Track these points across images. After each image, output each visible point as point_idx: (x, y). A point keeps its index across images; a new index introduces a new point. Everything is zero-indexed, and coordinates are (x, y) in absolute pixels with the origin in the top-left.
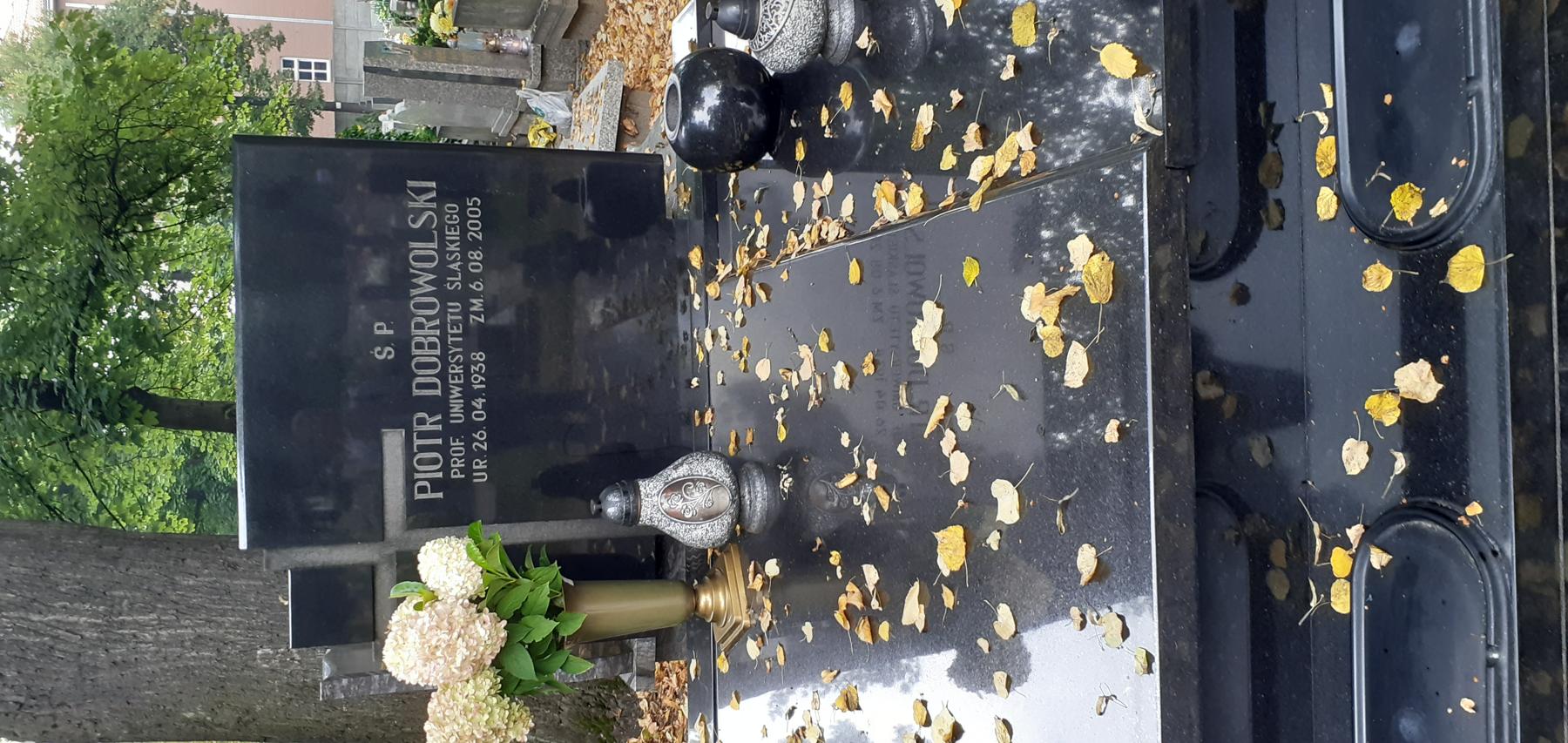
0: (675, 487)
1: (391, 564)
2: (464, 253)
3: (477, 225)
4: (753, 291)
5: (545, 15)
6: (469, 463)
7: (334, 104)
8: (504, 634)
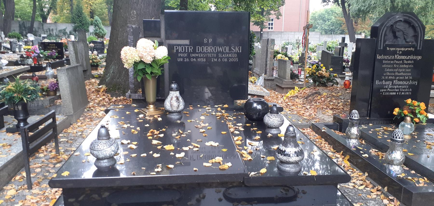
0: (178, 99)
1: (160, 41)
2: (226, 57)
3: (232, 60)
4: (219, 116)
5: (281, 80)
6: (182, 57)
7: (262, 31)
8: (148, 63)
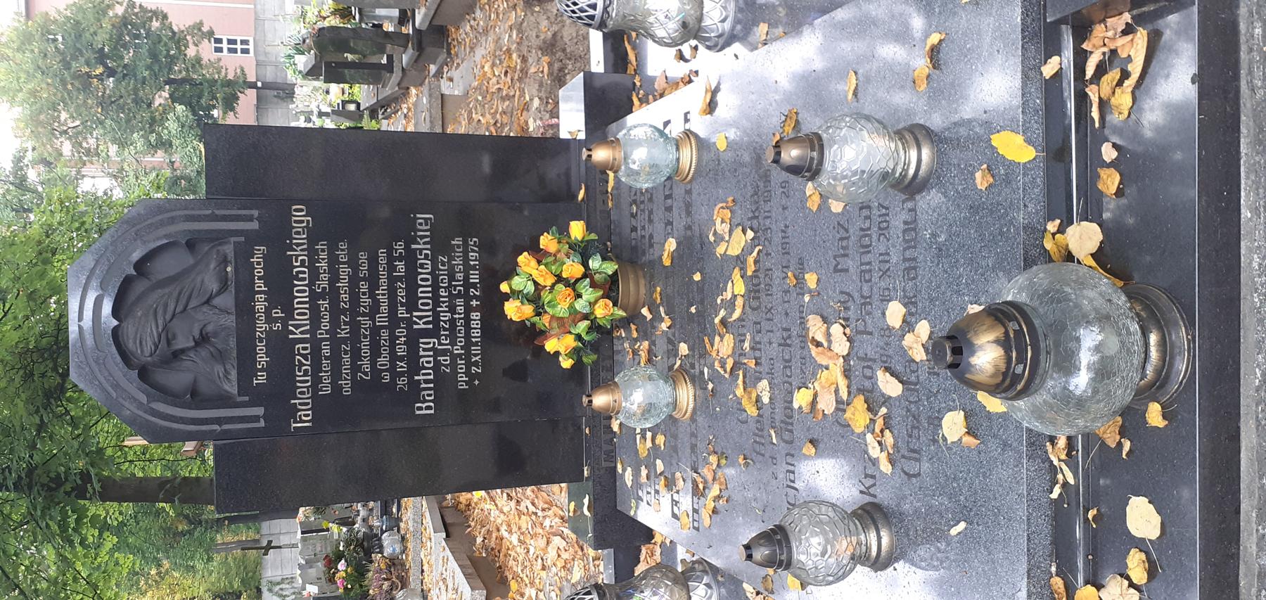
7: (256, 83)
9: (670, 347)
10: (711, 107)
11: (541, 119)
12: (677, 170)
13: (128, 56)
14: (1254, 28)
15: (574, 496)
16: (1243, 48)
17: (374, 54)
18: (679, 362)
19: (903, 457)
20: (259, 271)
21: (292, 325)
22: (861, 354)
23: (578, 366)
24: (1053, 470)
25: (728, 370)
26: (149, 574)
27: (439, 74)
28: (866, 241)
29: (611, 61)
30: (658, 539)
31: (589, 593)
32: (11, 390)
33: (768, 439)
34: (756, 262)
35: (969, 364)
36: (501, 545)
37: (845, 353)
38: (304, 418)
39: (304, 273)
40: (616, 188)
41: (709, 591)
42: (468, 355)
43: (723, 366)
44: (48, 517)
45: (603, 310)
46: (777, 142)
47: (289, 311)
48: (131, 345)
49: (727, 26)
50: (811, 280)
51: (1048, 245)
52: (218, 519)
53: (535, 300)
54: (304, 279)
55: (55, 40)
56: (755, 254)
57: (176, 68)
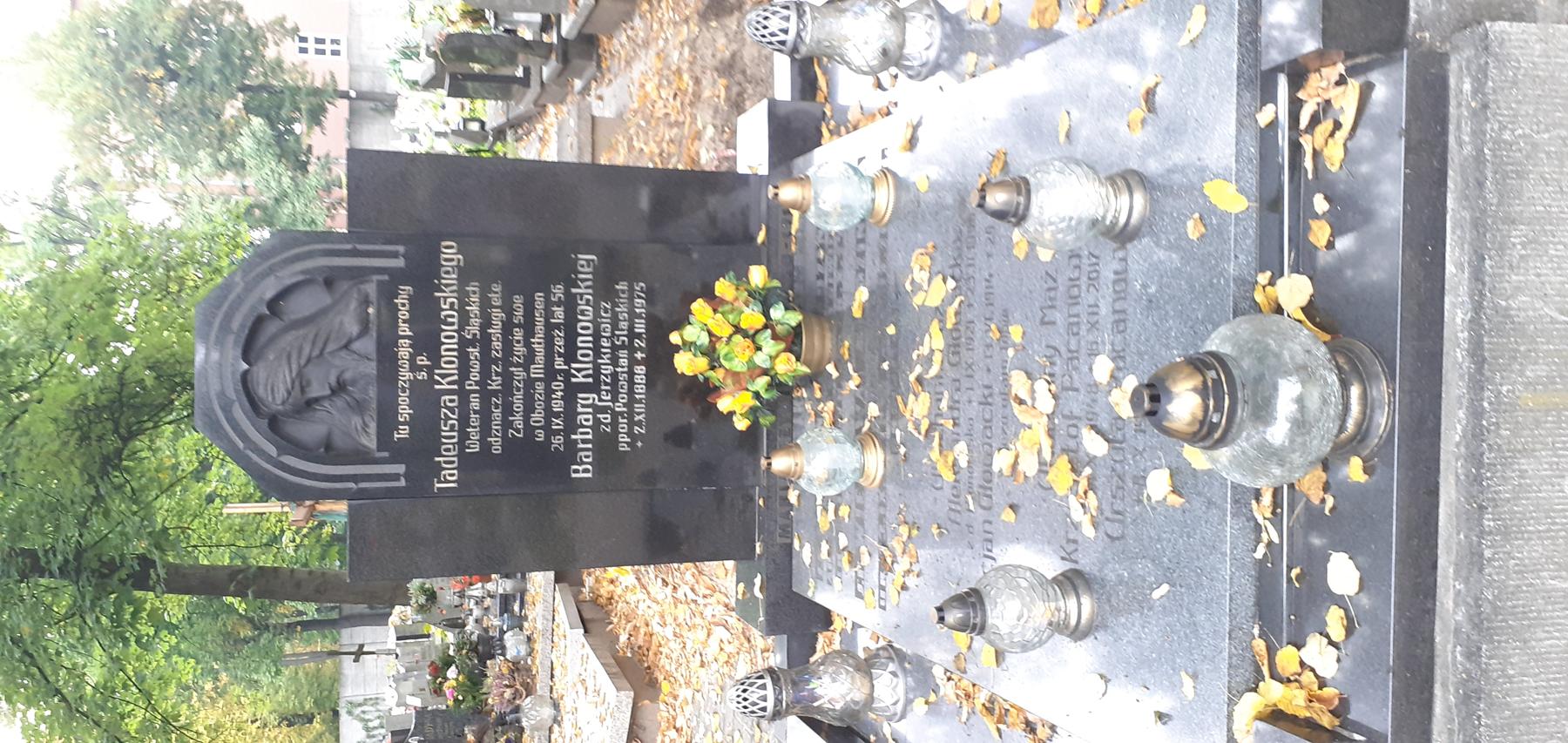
9: (859, 408)
10: (912, 143)
11: (715, 150)
12: (871, 211)
13: (194, 56)
14: (1463, 83)
15: (744, 578)
16: (1453, 102)
17: (503, 64)
18: (867, 425)
19: (1107, 519)
20: (404, 314)
21: (439, 375)
22: (1066, 412)
23: (754, 427)
24: (1258, 528)
25: (923, 432)
26: (203, 688)
27: (586, 90)
28: (1075, 291)
29: (798, 86)
30: (838, 624)
31: (761, 677)
32: (65, 455)
33: (965, 506)
34: (957, 314)
35: (1167, 412)
36: (650, 642)
37: (1050, 411)
38: (449, 477)
39: (453, 316)
40: (801, 230)
41: (895, 680)
42: (631, 414)
43: (917, 428)
44: (98, 609)
45: (786, 366)
46: (984, 185)
47: (435, 358)
48: (261, 392)
49: (932, 55)
50: (1016, 332)
51: (1259, 297)
52: (289, 625)
53: (710, 352)
54: (452, 324)
55: (106, 35)
56: (956, 304)
57: (252, 72)
